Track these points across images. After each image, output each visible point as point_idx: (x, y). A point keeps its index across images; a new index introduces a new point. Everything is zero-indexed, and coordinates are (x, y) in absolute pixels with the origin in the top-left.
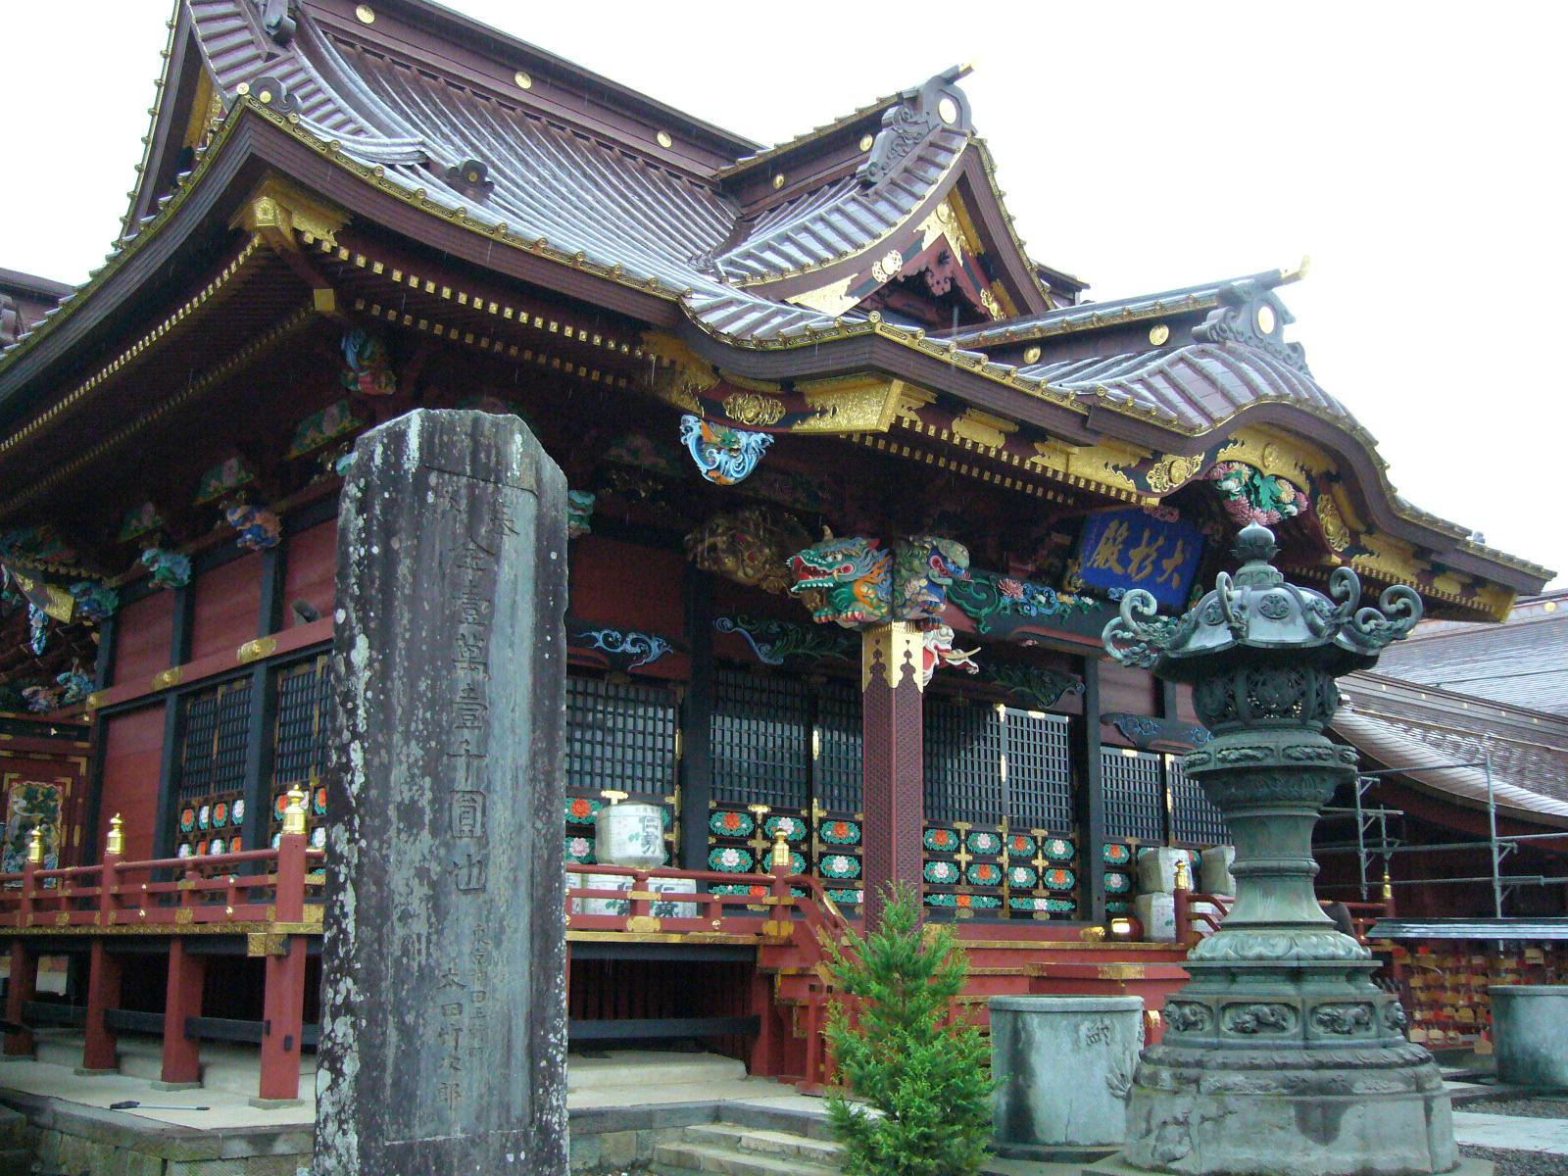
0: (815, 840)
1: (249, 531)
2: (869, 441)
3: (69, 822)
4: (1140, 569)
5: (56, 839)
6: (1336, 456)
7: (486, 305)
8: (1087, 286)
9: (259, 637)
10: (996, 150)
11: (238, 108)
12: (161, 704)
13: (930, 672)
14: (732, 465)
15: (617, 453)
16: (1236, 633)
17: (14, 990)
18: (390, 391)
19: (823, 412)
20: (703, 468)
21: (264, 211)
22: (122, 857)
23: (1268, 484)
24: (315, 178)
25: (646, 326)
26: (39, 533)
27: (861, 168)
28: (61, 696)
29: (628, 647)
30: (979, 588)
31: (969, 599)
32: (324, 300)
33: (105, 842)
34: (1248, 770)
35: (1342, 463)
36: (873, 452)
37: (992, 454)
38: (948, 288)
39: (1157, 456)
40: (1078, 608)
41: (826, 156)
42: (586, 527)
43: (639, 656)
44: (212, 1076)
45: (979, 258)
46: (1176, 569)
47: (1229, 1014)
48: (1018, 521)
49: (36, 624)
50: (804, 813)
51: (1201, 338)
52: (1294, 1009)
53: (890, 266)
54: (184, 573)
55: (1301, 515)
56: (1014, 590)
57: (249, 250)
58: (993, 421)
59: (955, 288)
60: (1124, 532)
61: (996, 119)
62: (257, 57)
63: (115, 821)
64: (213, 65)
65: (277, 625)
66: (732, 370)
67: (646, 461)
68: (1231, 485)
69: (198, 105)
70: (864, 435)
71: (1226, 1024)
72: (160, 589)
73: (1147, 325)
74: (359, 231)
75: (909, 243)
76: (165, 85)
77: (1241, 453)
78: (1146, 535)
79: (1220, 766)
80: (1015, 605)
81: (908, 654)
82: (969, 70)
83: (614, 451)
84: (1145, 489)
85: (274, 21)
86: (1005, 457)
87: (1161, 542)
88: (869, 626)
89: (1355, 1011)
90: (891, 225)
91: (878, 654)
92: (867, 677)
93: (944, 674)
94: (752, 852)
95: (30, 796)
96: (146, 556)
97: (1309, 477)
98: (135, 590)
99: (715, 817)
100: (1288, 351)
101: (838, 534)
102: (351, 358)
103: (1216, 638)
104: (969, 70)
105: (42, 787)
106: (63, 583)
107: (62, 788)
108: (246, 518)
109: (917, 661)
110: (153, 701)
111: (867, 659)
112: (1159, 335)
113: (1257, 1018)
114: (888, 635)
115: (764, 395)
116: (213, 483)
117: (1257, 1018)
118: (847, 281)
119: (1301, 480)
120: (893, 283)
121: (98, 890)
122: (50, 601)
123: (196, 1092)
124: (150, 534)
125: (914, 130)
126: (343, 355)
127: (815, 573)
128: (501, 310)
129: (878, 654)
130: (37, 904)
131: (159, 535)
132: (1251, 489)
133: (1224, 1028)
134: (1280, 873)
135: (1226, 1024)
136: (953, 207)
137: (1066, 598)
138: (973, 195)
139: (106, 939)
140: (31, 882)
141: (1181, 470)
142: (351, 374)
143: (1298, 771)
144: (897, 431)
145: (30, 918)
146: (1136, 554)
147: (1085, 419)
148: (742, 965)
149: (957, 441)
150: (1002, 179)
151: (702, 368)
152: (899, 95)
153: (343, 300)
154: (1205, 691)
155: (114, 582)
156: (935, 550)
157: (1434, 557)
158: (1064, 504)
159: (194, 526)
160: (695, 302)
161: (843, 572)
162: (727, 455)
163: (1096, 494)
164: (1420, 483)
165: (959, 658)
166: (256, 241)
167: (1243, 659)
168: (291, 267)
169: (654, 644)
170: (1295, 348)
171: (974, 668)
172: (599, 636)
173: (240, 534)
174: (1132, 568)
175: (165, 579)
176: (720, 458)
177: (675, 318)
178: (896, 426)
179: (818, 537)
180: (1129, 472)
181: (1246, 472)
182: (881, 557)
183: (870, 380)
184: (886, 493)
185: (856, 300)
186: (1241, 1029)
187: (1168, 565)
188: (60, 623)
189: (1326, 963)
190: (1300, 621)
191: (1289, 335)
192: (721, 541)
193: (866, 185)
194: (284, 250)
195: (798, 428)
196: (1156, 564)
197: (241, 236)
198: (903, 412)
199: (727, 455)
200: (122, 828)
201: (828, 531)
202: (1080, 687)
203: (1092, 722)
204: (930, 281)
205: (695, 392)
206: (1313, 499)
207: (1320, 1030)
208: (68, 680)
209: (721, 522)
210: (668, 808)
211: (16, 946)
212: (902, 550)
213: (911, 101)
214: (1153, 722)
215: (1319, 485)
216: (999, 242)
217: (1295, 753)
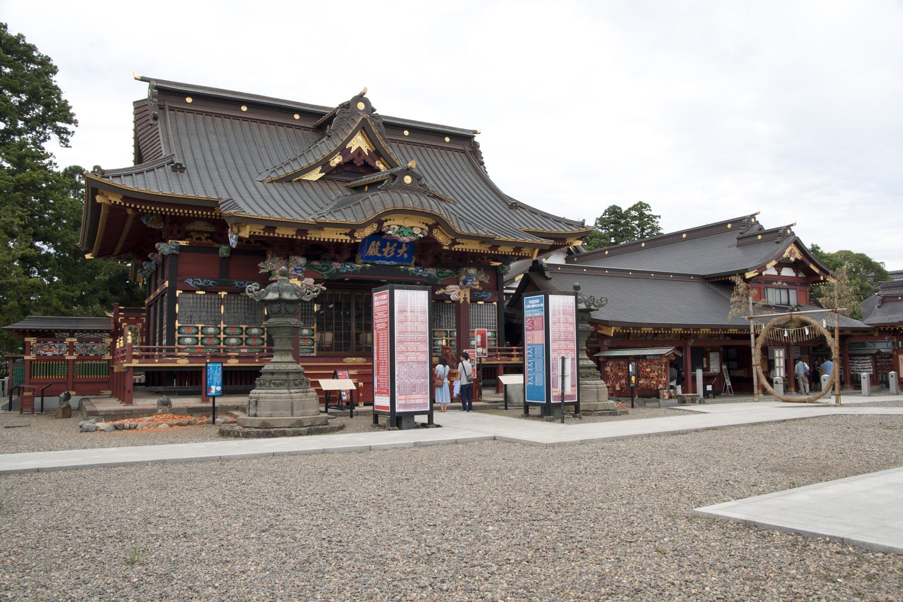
3: (142, 336)
53: (337, 160)
75: (343, 150)
105: (133, 327)
146: (386, 250)
180: (346, 234)
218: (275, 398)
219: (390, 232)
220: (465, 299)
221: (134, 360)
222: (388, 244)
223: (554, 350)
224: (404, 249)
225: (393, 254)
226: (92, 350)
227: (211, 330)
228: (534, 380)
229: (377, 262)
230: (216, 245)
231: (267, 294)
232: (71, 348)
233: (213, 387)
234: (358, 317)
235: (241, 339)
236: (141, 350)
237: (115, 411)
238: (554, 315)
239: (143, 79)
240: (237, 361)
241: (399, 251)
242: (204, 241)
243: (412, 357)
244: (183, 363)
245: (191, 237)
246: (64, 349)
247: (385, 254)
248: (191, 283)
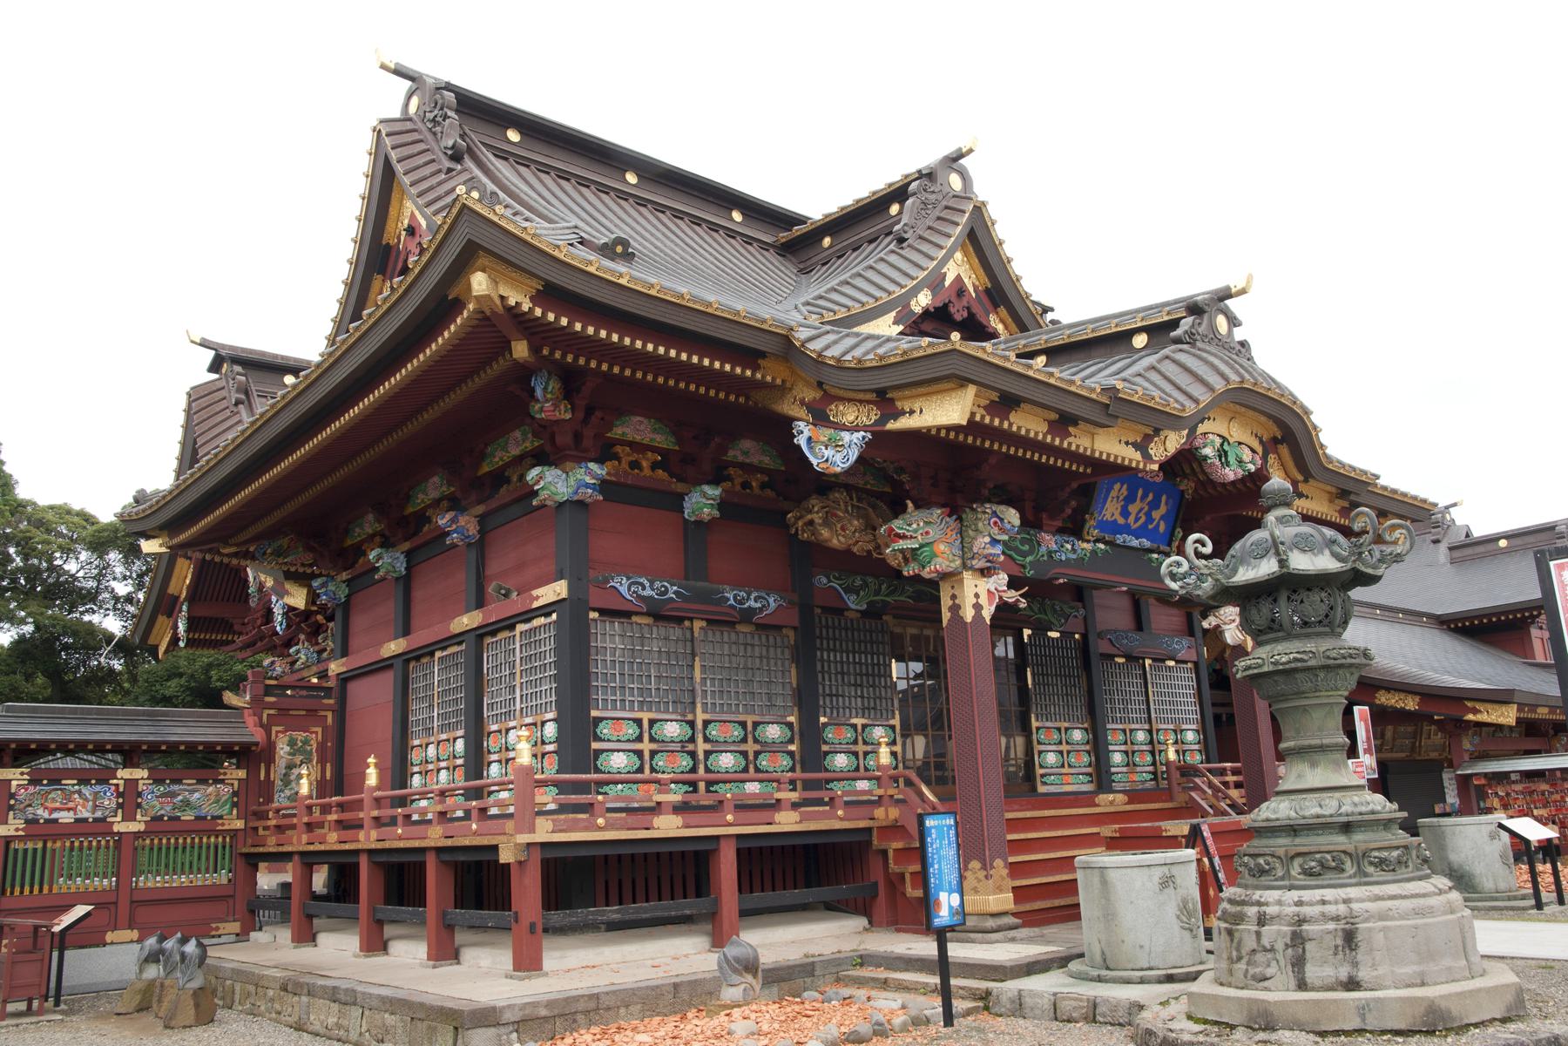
0: (700, 739)
1: (455, 531)
2: (943, 433)
3: (322, 762)
4: (1137, 520)
5: (316, 774)
6: (1279, 423)
7: (656, 348)
8: (1052, 310)
9: (467, 611)
10: (993, 211)
11: (458, 206)
12: (391, 666)
13: (993, 609)
14: (838, 458)
15: (734, 454)
16: (1283, 563)
17: (296, 893)
18: (568, 416)
19: (912, 412)
20: (814, 462)
21: (479, 283)
22: (378, 788)
23: (1232, 447)
24: (514, 255)
25: (762, 354)
26: (285, 542)
27: (896, 228)
28: (293, 663)
29: (752, 603)
30: (1023, 541)
31: (1016, 550)
32: (521, 350)
33: (363, 776)
34: (1295, 670)
35: (1288, 431)
36: (946, 441)
37: (1040, 437)
38: (965, 314)
39: (1157, 431)
40: (1094, 552)
41: (865, 220)
42: (716, 513)
43: (761, 609)
44: (468, 955)
45: (987, 291)
46: (1162, 518)
47: (1297, 862)
48: (1054, 491)
49: (278, 611)
50: (690, 717)
51: (1178, 341)
52: (1350, 855)
53: (923, 300)
54: (401, 567)
55: (1258, 470)
56: (1049, 541)
57: (465, 314)
58: (1039, 410)
59: (971, 315)
60: (1124, 491)
61: (994, 186)
62: (440, 171)
63: (371, 760)
64: (407, 180)
65: (480, 603)
66: (832, 386)
67: (754, 460)
68: (1208, 451)
69: (393, 211)
70: (939, 429)
71: (1295, 870)
72: (383, 579)
73: (1128, 335)
74: (550, 294)
75: (935, 282)
76: (367, 199)
77: (1214, 429)
78: (1140, 493)
79: (1271, 668)
80: (1050, 553)
81: (977, 596)
82: (971, 151)
83: (731, 453)
84: (1147, 457)
85: (450, 143)
86: (1049, 439)
87: (1150, 497)
88: (945, 576)
89: (1395, 853)
90: (923, 269)
91: (954, 597)
92: (946, 616)
93: (1003, 609)
94: (744, 754)
95: (292, 743)
96: (372, 555)
97: (1261, 442)
98: (363, 579)
99: (601, 725)
100: (1238, 347)
101: (917, 507)
102: (539, 393)
103: (1267, 568)
104: (971, 151)
105: (300, 736)
106: (302, 579)
107: (315, 736)
108: (453, 521)
109: (983, 600)
110: (384, 665)
111: (946, 602)
112: (1140, 341)
113: (1322, 864)
114: (961, 581)
115: (861, 402)
116: (421, 496)
117: (1322, 864)
118: (893, 314)
119: (1256, 445)
120: (926, 314)
121: (361, 815)
122: (287, 593)
123: (456, 967)
124: (373, 536)
125: (932, 197)
126: (533, 390)
127: (904, 537)
128: (667, 352)
129: (954, 597)
130: (310, 827)
131: (378, 539)
132: (1222, 454)
133: (1293, 873)
134: (1322, 749)
135: (1295, 870)
136: (966, 254)
137: (1085, 545)
138: (979, 241)
139: (371, 852)
140: (304, 811)
141: (1173, 442)
142: (538, 406)
143: (1331, 668)
144: (972, 426)
145: (305, 838)
146: (1133, 508)
147: (1107, 406)
148: (859, 843)
149: (1014, 428)
150: (1001, 231)
151: (808, 384)
152: (919, 171)
153: (535, 349)
154: (1254, 611)
155: (345, 576)
156: (994, 513)
157: (1352, 497)
158: (1085, 473)
159: (405, 526)
160: (802, 334)
161: (922, 536)
162: (833, 449)
164: (1344, 440)
165: (1011, 596)
166: (471, 307)
167: (1289, 584)
168: (498, 325)
169: (771, 600)
170: (1243, 344)
171: (1023, 604)
172: (730, 596)
173: (448, 533)
174: (1131, 519)
175: (387, 572)
176: (828, 453)
177: (786, 347)
178: (971, 421)
179: (904, 510)
180: (1136, 446)
181: (1218, 441)
182: (951, 520)
183: (951, 385)
184: (950, 473)
185: (901, 328)
186: (1308, 873)
187: (1156, 515)
188: (295, 609)
189: (1366, 817)
190: (1327, 552)
191: (1239, 334)
192: (817, 518)
193: (901, 240)
194: (493, 312)
195: (891, 426)
196: (1148, 515)
197: (457, 305)
198: (975, 409)
199: (833, 449)
200: (376, 765)
201: (910, 504)
202: (1082, 611)
203: (1091, 638)
204: (952, 310)
205: (802, 403)
206: (1265, 458)
207: (1371, 869)
208: (298, 652)
209: (815, 503)
210: (790, 725)
211: (296, 858)
212: (968, 516)
213: (928, 176)
214: (1136, 636)
215: (1269, 446)
216: (1002, 279)
217: (1333, 654)
218: (1418, 913)
221: (540, 821)
226: (187, 804)
229: (1120, 539)
230: (680, 487)
231: (1235, 571)
232: (129, 800)
233: (943, 896)
235: (744, 754)
236: (562, 787)
237: (550, 1004)
239: (399, 72)
240: (677, 820)
242: (647, 472)
244: (668, 826)
245: (617, 457)
246: (109, 801)
248: (623, 590)
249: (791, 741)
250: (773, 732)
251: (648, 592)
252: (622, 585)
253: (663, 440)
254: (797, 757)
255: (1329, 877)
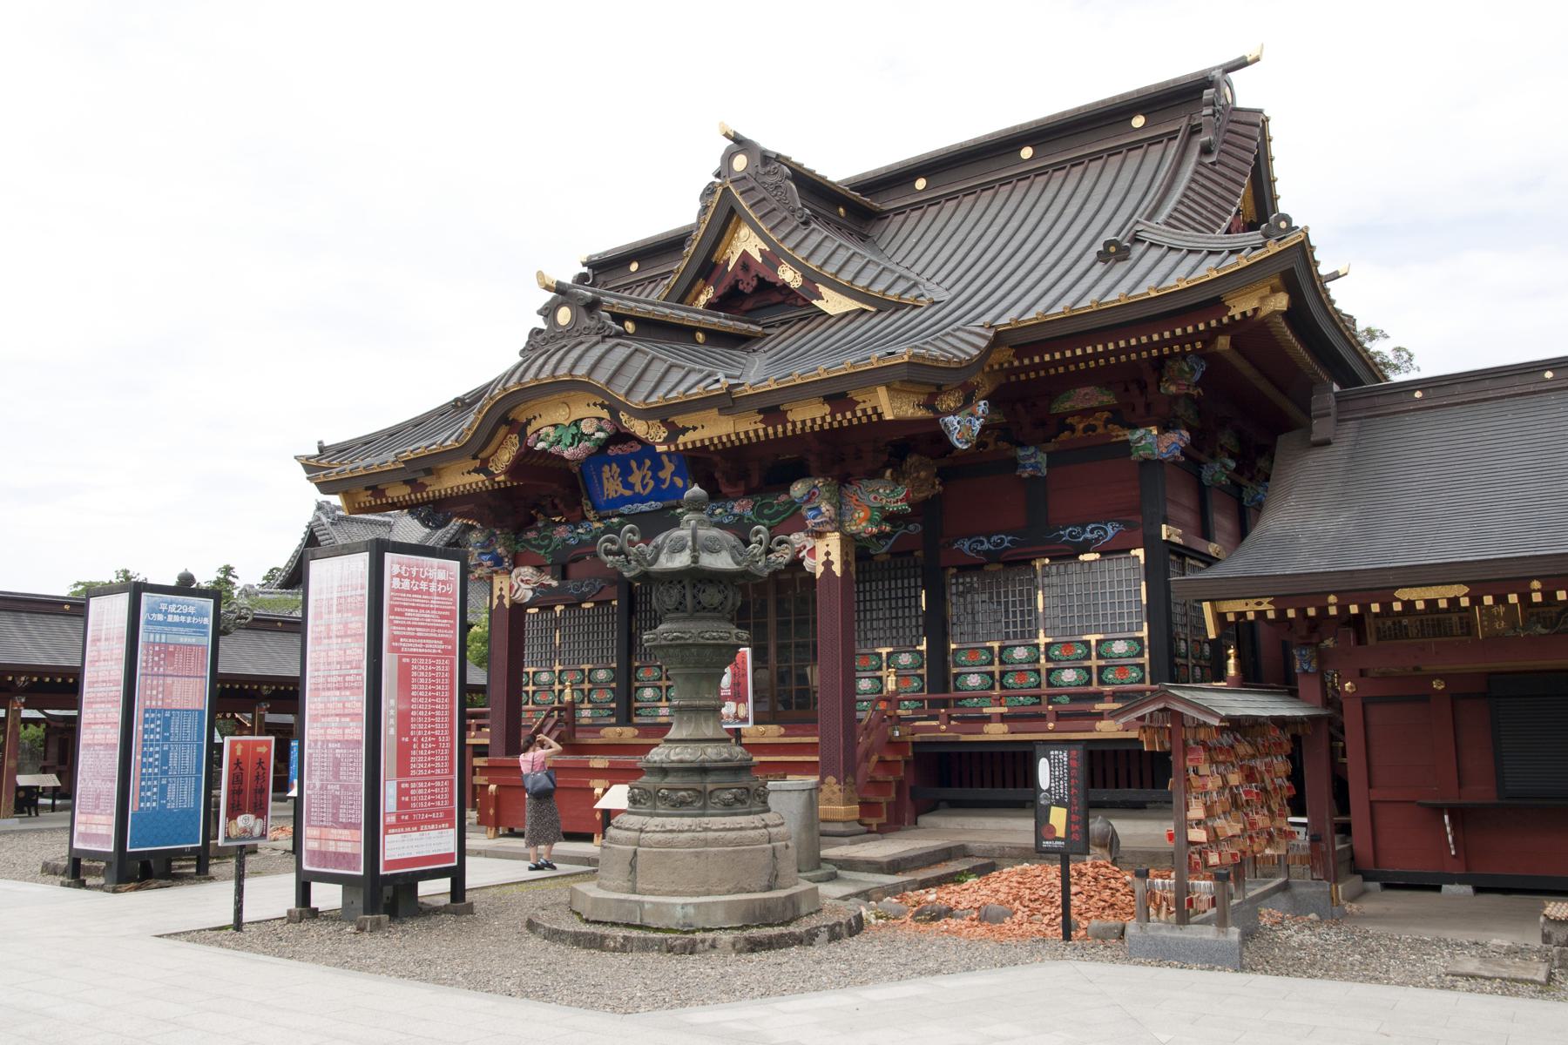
4: (644, 487)
33: (1226, 668)
43: (1097, 540)
81: (828, 554)
146: (635, 479)
163: (440, 499)
180: (477, 471)
196: (655, 477)
200: (1238, 657)
210: (1140, 640)
219: (540, 445)
220: (828, 564)
222: (634, 464)
223: (315, 718)
224: (670, 468)
225: (652, 483)
227: (545, 677)
228: (163, 790)
234: (783, 625)
238: (319, 616)
240: (1004, 727)
241: (662, 475)
243: (99, 738)
244: (996, 732)
247: (638, 488)
249: (921, 666)
250: (602, 675)
251: (986, 546)
252: (965, 545)
253: (1108, 399)
254: (1147, 669)
255: (739, 807)
